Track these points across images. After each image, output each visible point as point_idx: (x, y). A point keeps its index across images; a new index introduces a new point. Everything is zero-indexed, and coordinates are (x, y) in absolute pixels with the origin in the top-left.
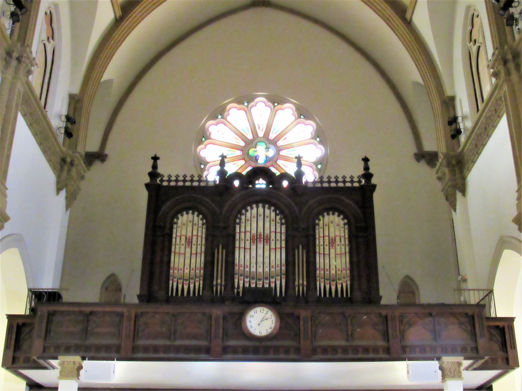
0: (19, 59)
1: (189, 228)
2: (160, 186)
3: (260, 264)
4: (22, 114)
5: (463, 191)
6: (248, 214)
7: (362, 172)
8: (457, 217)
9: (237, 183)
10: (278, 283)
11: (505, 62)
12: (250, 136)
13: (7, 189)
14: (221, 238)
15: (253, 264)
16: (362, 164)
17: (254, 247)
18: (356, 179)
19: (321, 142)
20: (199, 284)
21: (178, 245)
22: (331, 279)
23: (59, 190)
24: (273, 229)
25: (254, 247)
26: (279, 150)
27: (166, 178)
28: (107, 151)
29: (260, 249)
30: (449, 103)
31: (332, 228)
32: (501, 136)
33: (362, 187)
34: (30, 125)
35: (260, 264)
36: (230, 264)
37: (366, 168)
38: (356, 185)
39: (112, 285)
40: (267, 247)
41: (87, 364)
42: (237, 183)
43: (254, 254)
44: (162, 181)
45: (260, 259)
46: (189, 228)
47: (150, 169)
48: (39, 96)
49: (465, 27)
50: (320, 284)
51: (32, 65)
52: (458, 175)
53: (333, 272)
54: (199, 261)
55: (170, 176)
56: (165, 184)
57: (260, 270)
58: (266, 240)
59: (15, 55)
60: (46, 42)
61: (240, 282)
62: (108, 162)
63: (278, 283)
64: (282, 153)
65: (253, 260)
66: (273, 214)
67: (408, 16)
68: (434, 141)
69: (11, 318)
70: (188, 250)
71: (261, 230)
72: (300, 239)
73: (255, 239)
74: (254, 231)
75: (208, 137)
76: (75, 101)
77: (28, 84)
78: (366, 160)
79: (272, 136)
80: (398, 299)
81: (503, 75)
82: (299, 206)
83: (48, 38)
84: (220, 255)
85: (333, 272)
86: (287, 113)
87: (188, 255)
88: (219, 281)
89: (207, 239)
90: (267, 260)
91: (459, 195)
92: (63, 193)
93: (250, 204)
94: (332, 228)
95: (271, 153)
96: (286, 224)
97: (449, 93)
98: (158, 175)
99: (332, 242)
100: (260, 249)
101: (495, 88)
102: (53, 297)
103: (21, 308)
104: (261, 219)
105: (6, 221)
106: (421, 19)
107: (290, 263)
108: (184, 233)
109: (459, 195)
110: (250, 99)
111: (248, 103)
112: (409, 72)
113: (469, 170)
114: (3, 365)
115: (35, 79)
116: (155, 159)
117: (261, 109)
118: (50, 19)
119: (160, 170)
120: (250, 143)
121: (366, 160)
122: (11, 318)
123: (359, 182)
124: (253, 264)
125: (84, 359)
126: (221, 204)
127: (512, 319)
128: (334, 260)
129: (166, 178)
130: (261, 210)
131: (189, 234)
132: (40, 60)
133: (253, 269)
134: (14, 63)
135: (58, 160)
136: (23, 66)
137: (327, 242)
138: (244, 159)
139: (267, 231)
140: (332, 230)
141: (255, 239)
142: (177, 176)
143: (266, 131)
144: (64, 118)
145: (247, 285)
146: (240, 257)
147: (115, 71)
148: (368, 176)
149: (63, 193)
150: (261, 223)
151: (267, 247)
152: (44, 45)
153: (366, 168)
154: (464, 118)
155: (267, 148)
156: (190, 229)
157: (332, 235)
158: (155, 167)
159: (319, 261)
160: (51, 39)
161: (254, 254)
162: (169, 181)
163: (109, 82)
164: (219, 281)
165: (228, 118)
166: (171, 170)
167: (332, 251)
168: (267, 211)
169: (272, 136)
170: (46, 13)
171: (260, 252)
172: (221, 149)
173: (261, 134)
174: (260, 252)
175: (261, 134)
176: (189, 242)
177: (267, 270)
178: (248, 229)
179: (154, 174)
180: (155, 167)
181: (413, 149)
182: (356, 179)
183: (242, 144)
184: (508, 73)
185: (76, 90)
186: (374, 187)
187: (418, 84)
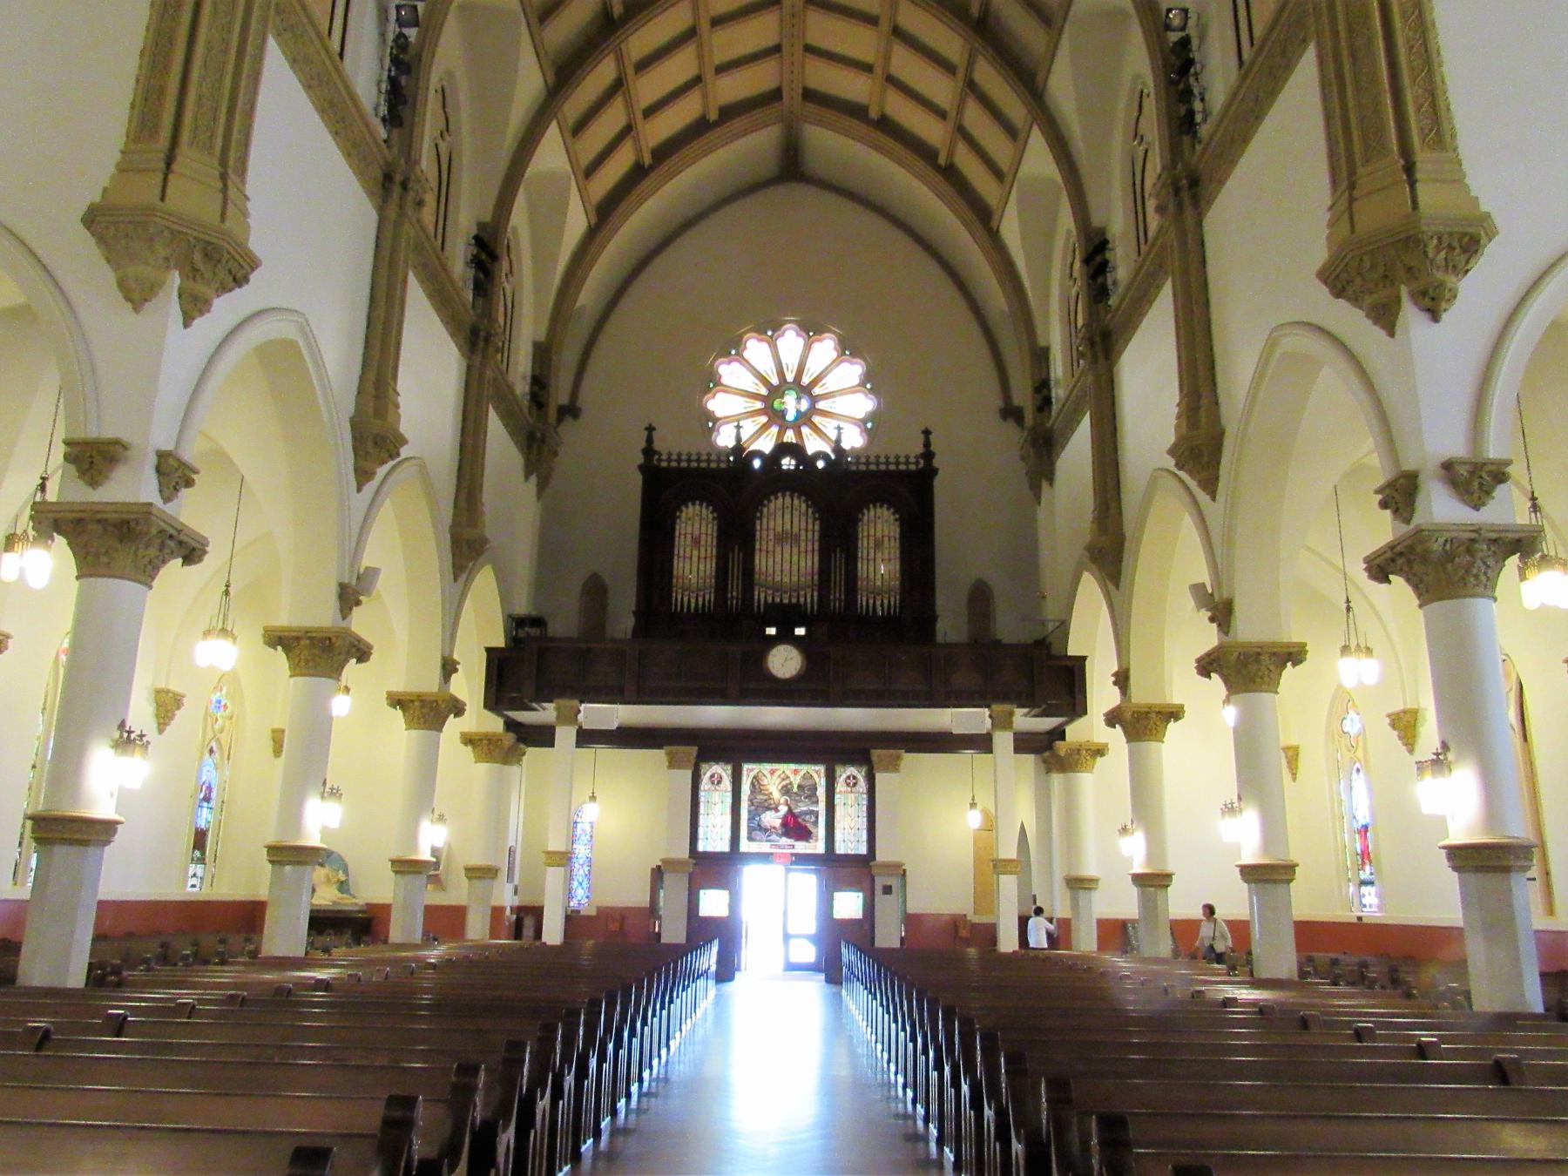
0: (404, 186)
1: (695, 526)
2: (658, 469)
3: (786, 572)
5: (1051, 480)
6: (772, 505)
7: (920, 450)
8: (1042, 513)
9: (757, 463)
10: (809, 598)
11: (1177, 191)
12: (775, 381)
14: (736, 537)
15: (778, 572)
16: (921, 439)
17: (778, 549)
18: (912, 460)
19: (871, 391)
20: (710, 596)
21: (682, 545)
22: (877, 592)
23: (527, 477)
24: (803, 525)
25: (778, 549)
26: (814, 400)
27: (664, 457)
28: (580, 403)
29: (786, 555)
30: (1041, 356)
31: (880, 530)
32: (1303, 86)
33: (919, 472)
34: (502, 418)
35: (786, 572)
36: (748, 572)
37: (927, 444)
38: (913, 467)
39: (596, 591)
40: (795, 550)
41: (583, 707)
42: (757, 463)
43: (778, 558)
44: (660, 460)
45: (786, 566)
46: (695, 526)
47: (643, 445)
49: (1064, 259)
50: (863, 600)
53: (879, 583)
54: (709, 567)
55: (670, 454)
56: (664, 464)
57: (786, 580)
58: (794, 539)
59: (398, 178)
61: (761, 596)
62: (585, 418)
63: (809, 598)
64: (821, 405)
65: (778, 568)
66: (804, 506)
67: (994, 224)
68: (1023, 395)
69: (489, 650)
70: (695, 553)
71: (788, 527)
72: (838, 539)
73: (781, 539)
74: (779, 529)
75: (718, 383)
76: (543, 353)
78: (927, 433)
79: (806, 380)
81: (1171, 207)
82: (838, 491)
84: (736, 558)
85: (879, 583)
87: (695, 559)
88: (734, 593)
89: (719, 538)
90: (795, 567)
91: (1045, 484)
92: (533, 479)
93: (774, 493)
94: (880, 530)
95: (804, 405)
96: (820, 519)
97: (1042, 342)
98: (656, 452)
99: (878, 545)
100: (786, 555)
101: (1160, 230)
102: (537, 622)
103: (499, 641)
104: (788, 511)
106: (1011, 229)
107: (824, 572)
108: (689, 530)
109: (1045, 484)
110: (777, 326)
111: (774, 331)
112: (996, 299)
113: (1058, 456)
114: (486, 707)
116: (650, 429)
117: (790, 342)
119: (657, 445)
120: (776, 392)
121: (927, 433)
122: (489, 650)
123: (917, 463)
124: (778, 572)
125: (582, 702)
126: (736, 488)
127: (1084, 658)
128: (880, 566)
129: (664, 457)
130: (788, 500)
131: (696, 532)
133: (778, 578)
134: (397, 191)
135: (379, 174)
136: (411, 195)
137: (872, 544)
139: (796, 529)
140: (879, 526)
141: (781, 539)
142: (679, 454)
143: (795, 387)
144: (529, 380)
145: (770, 599)
146: (760, 562)
147: (589, 296)
148: (928, 455)
149: (533, 479)
150: (787, 517)
151: (795, 550)
153: (927, 444)
154: (1057, 382)
155: (799, 399)
156: (697, 525)
157: (879, 534)
158: (650, 440)
159: (862, 567)
161: (778, 558)
162: (669, 460)
163: (583, 308)
164: (734, 593)
165: (746, 354)
166: (671, 444)
167: (879, 555)
168: (796, 502)
169: (806, 380)
171: (787, 556)
172: (735, 418)
173: (790, 377)
174: (787, 556)
175: (790, 377)
176: (696, 542)
177: (795, 579)
178: (772, 525)
179: (649, 451)
180: (650, 440)
181: (999, 403)
182: (912, 460)
183: (764, 391)
184: (1180, 207)
185: (542, 337)
186: (935, 472)
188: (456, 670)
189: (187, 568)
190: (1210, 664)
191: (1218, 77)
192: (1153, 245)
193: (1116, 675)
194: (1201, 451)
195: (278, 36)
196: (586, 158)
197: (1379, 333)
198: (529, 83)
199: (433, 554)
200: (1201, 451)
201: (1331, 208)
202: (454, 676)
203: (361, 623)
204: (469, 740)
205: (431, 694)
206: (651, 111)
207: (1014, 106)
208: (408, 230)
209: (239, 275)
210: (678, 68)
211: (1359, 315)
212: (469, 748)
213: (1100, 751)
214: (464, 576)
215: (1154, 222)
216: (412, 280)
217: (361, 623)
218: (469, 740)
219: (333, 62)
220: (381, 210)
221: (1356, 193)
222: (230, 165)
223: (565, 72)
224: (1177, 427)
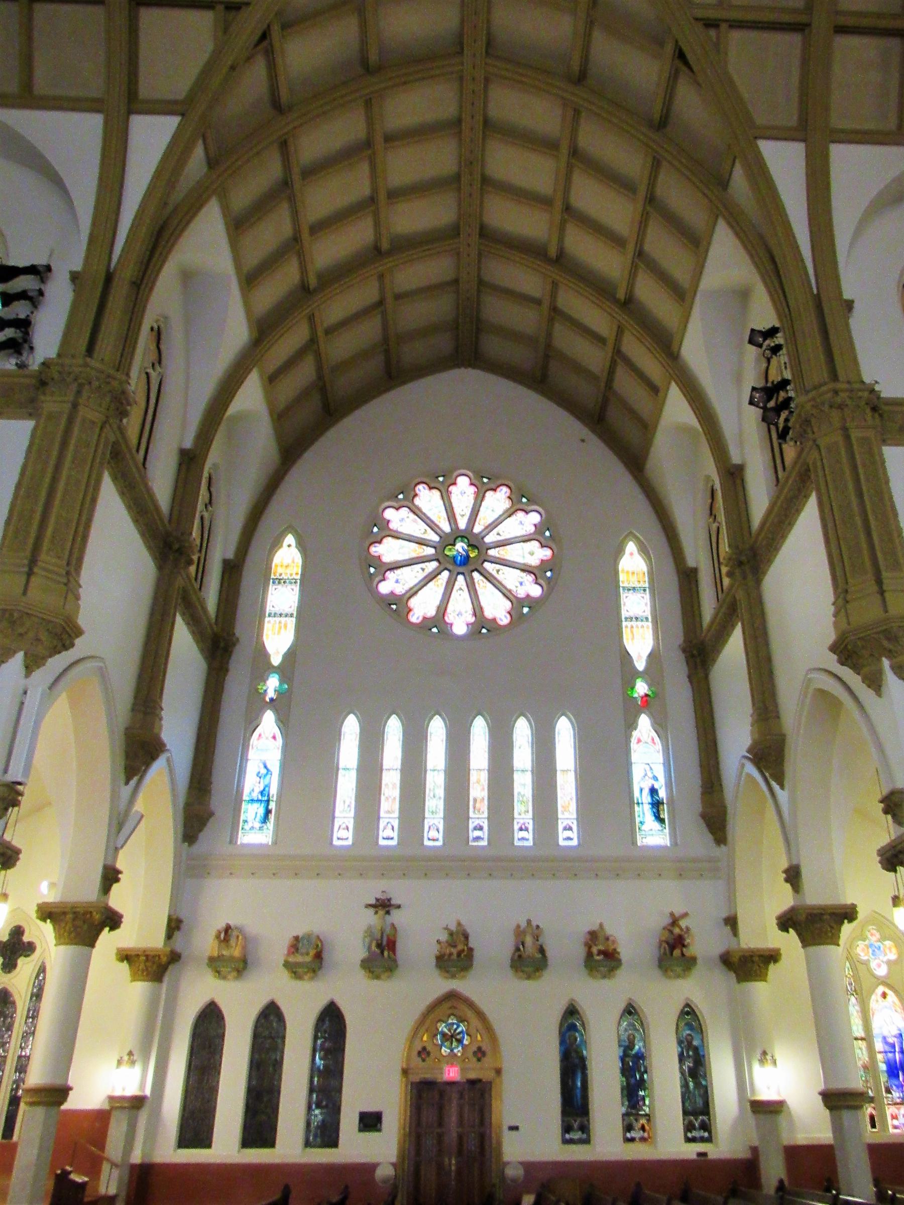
4: (110, 474)
13: (80, 586)
32: (808, 525)
48: (135, 447)
51: (129, 404)
52: (750, 577)
60: (150, 371)
77: (121, 430)
80: (290, 953)
83: (153, 365)
86: (497, 501)
105: (77, 637)
115: (132, 424)
118: (158, 334)
132: (141, 398)
138: (438, 560)
152: (147, 374)
160: (157, 366)
170: (152, 329)
171: (523, 755)
174: (523, 755)
187: (688, 429)
188: (117, 880)
189: (112, 933)
190: (896, 856)
191: (760, 497)
192: (728, 594)
193: (786, 871)
194: (769, 756)
195: (183, 615)
196: (253, 259)
197: (871, 692)
198: (236, 332)
199: (105, 753)
200: (769, 756)
201: (833, 604)
202: (115, 887)
203: (118, 899)
204: (126, 956)
205: (156, 950)
206: (320, 227)
207: (652, 366)
208: (179, 582)
209: (68, 642)
210: (351, 185)
211: (859, 678)
212: (125, 965)
213: (772, 957)
214: (136, 779)
215: (726, 581)
216: (179, 620)
217: (118, 899)
218: (126, 956)
219: (137, 468)
220: (160, 568)
221: (849, 597)
222: (73, 563)
223: (264, 330)
224: (752, 733)
